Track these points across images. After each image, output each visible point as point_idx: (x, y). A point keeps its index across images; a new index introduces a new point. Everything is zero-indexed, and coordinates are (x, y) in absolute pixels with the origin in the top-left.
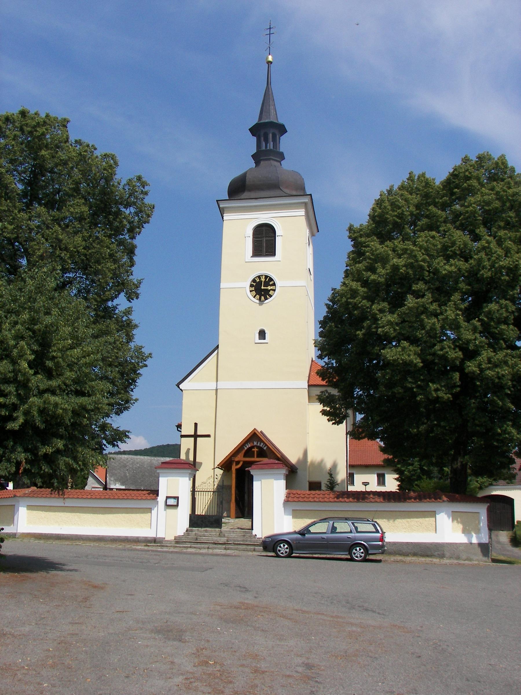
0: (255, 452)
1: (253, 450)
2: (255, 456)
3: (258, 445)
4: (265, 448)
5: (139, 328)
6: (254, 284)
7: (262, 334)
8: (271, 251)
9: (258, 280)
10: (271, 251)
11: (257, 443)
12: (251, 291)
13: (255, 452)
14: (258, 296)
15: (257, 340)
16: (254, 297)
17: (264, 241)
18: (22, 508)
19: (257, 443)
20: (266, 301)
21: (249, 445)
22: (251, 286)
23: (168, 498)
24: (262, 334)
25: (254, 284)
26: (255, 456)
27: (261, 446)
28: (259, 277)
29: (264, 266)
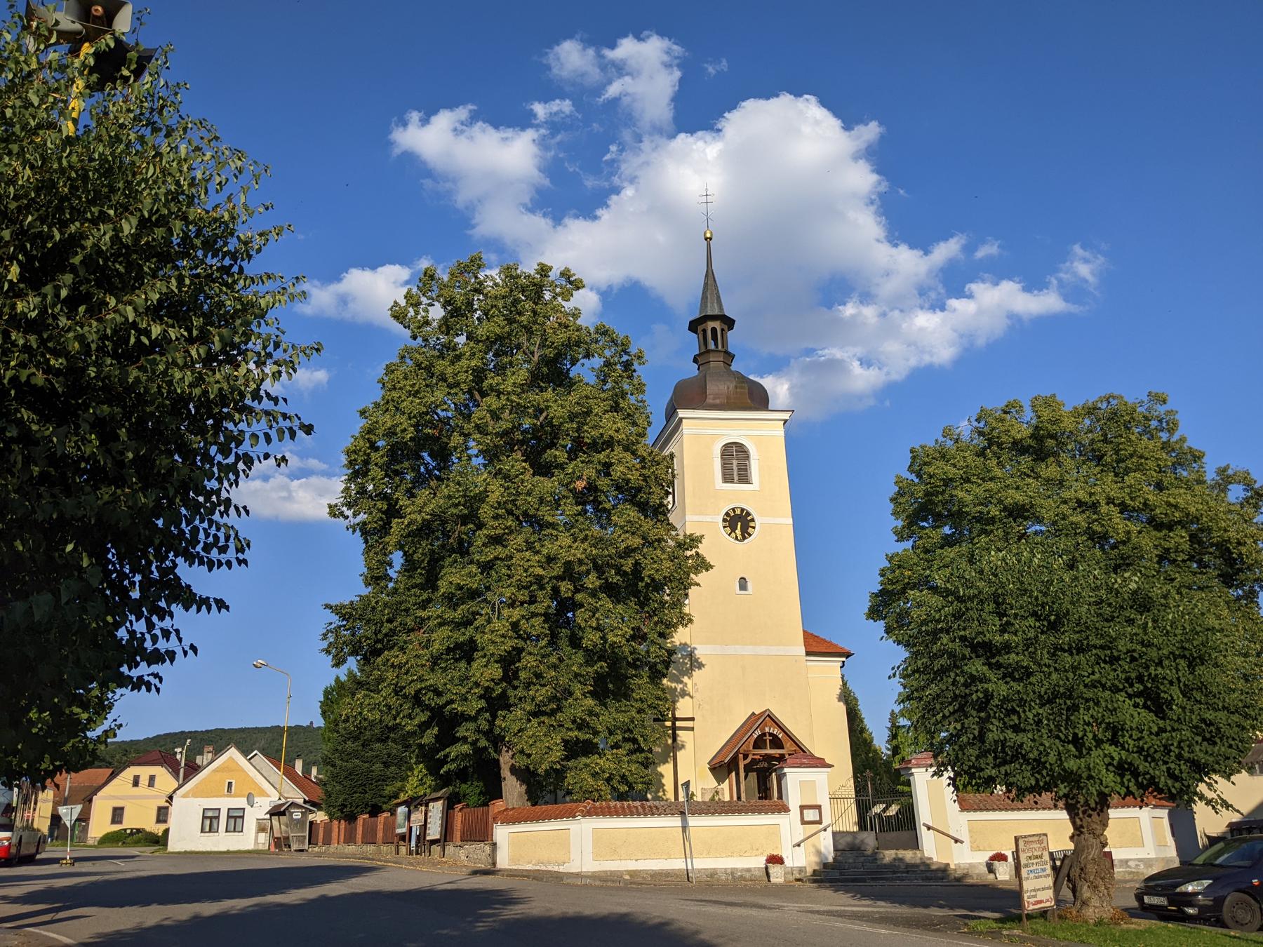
8: (744, 478)
10: (744, 478)
14: (752, 524)
17: (735, 462)
22: (724, 520)
23: (802, 808)
28: (733, 510)
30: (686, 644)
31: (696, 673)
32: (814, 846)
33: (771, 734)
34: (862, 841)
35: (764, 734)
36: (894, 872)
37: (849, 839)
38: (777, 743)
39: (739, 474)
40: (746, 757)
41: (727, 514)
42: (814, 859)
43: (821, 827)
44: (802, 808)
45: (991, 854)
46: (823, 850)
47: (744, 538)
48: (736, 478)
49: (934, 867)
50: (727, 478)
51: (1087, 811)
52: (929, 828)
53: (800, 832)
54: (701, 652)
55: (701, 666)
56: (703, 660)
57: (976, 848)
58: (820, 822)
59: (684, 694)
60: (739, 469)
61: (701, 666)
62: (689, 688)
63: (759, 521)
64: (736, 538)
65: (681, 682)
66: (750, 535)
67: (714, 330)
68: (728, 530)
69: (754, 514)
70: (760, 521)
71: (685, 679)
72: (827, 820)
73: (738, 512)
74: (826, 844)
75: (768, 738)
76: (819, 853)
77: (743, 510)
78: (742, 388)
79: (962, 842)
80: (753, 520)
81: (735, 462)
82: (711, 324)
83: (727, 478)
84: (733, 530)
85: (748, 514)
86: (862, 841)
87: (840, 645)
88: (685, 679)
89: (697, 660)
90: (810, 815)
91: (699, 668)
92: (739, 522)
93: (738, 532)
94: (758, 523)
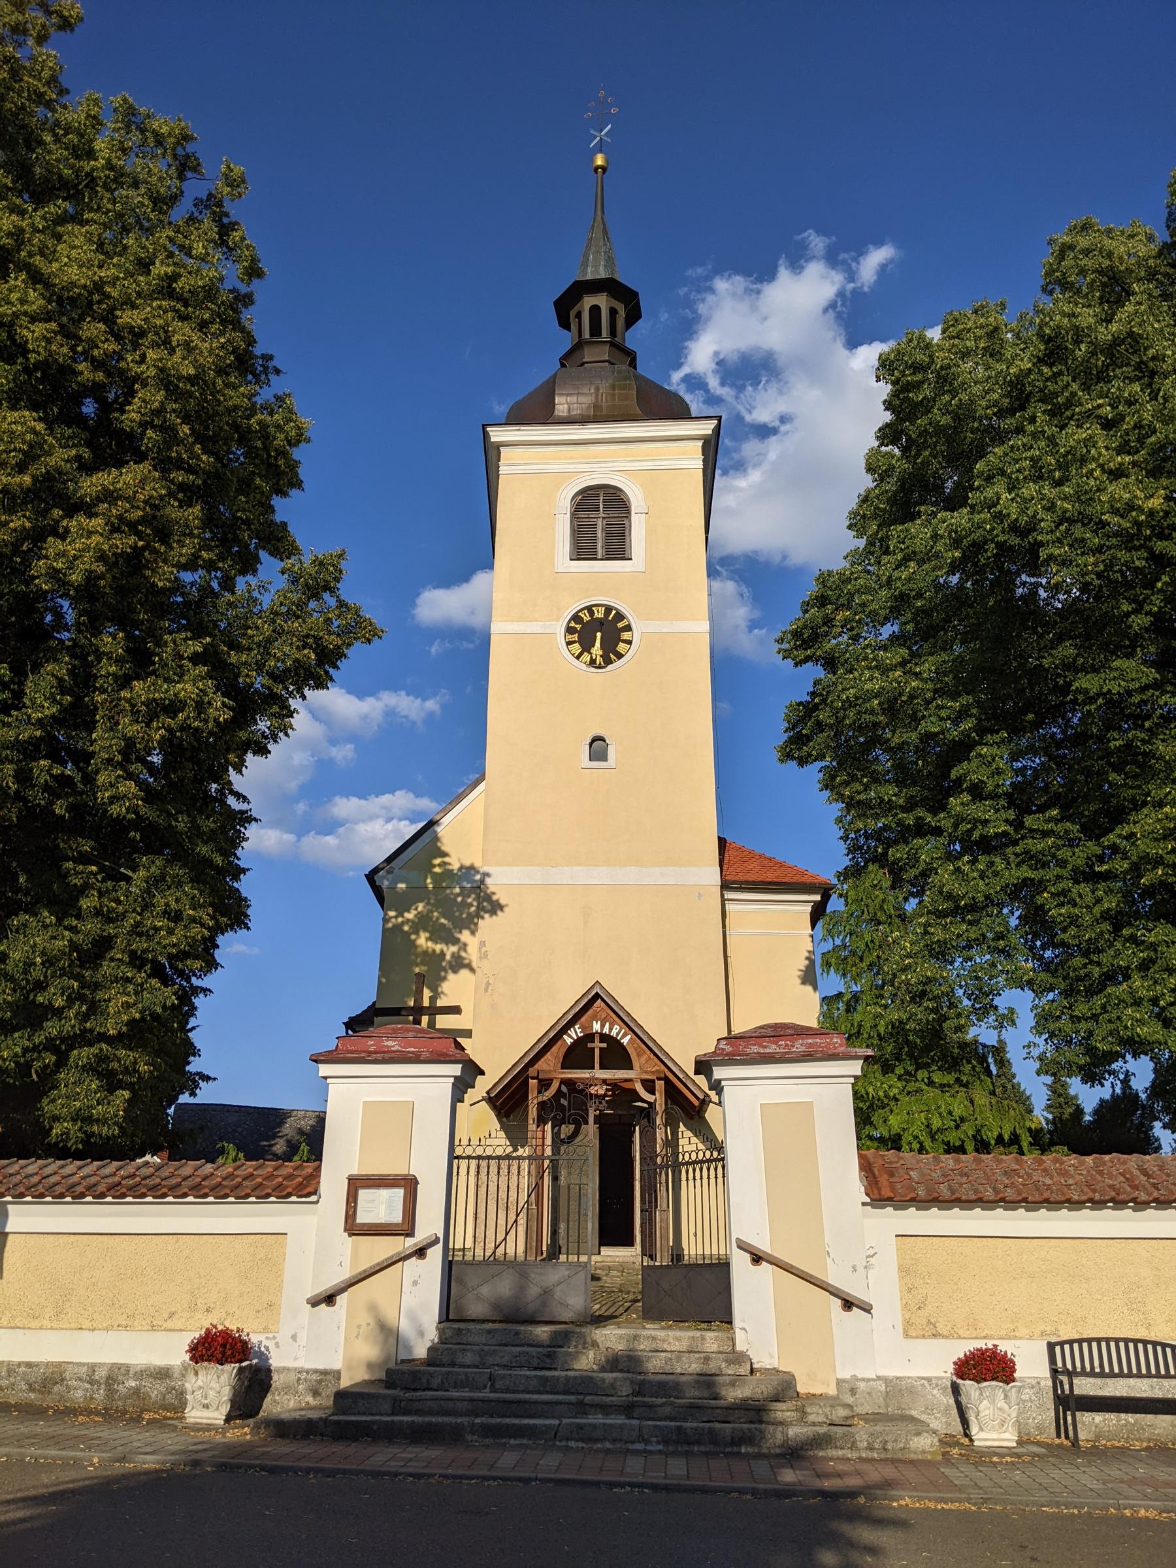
0: (597, 1052)
1: (590, 1045)
2: (597, 1065)
3: (606, 1030)
4: (625, 1041)
5: (287, 500)
6: (578, 627)
7: (598, 748)
8: (618, 549)
9: (587, 618)
10: (618, 549)
11: (603, 1026)
12: (569, 643)
13: (597, 1052)
14: (626, 636)
15: (586, 761)
16: (578, 658)
17: (601, 521)
18: (395, 1221)
19: (603, 1026)
20: (610, 667)
21: (576, 1033)
22: (570, 630)
23: (356, 1184)
24: (598, 748)
25: (578, 627)
26: (597, 1065)
27: (614, 1033)
28: (589, 609)
29: (600, 582)
30: (472, 868)
31: (486, 923)
32: (373, 1308)
33: (604, 1038)
34: (547, 1292)
35: (590, 1037)
36: (582, 1408)
37: (504, 1287)
38: (616, 1055)
39: (607, 544)
40: (545, 1084)
41: (576, 618)
42: (368, 1351)
43: (410, 1242)
44: (356, 1184)
45: (962, 1349)
46: (405, 1326)
47: (608, 662)
48: (600, 552)
49: (734, 1395)
50: (582, 550)
51: (408, 934)
52: (757, 1258)
53: (347, 1256)
54: (499, 882)
55: (496, 908)
56: (501, 896)
57: (920, 1327)
58: (407, 1229)
59: (459, 963)
60: (608, 534)
61: (496, 908)
62: (472, 953)
63: (641, 628)
64: (592, 662)
65: (456, 941)
66: (620, 656)
67: (595, 310)
68: (576, 648)
69: (632, 617)
70: (642, 628)
71: (465, 936)
72: (429, 1223)
73: (599, 614)
74: (415, 1303)
75: (598, 1045)
76: (387, 1332)
77: (609, 609)
78: (624, 387)
79: (867, 1309)
80: (628, 628)
81: (601, 521)
82: (588, 301)
83: (582, 550)
84: (587, 647)
85: (620, 616)
86: (547, 1292)
87: (801, 866)
88: (465, 936)
89: (489, 898)
90: (381, 1206)
91: (493, 912)
92: (600, 633)
93: (597, 650)
94: (636, 635)
